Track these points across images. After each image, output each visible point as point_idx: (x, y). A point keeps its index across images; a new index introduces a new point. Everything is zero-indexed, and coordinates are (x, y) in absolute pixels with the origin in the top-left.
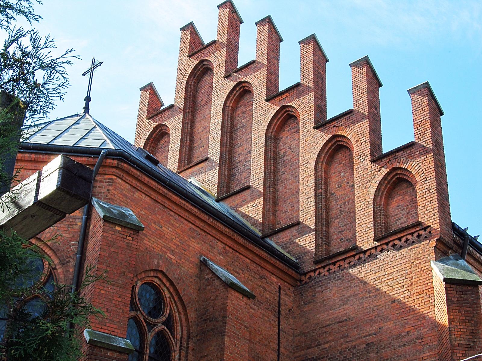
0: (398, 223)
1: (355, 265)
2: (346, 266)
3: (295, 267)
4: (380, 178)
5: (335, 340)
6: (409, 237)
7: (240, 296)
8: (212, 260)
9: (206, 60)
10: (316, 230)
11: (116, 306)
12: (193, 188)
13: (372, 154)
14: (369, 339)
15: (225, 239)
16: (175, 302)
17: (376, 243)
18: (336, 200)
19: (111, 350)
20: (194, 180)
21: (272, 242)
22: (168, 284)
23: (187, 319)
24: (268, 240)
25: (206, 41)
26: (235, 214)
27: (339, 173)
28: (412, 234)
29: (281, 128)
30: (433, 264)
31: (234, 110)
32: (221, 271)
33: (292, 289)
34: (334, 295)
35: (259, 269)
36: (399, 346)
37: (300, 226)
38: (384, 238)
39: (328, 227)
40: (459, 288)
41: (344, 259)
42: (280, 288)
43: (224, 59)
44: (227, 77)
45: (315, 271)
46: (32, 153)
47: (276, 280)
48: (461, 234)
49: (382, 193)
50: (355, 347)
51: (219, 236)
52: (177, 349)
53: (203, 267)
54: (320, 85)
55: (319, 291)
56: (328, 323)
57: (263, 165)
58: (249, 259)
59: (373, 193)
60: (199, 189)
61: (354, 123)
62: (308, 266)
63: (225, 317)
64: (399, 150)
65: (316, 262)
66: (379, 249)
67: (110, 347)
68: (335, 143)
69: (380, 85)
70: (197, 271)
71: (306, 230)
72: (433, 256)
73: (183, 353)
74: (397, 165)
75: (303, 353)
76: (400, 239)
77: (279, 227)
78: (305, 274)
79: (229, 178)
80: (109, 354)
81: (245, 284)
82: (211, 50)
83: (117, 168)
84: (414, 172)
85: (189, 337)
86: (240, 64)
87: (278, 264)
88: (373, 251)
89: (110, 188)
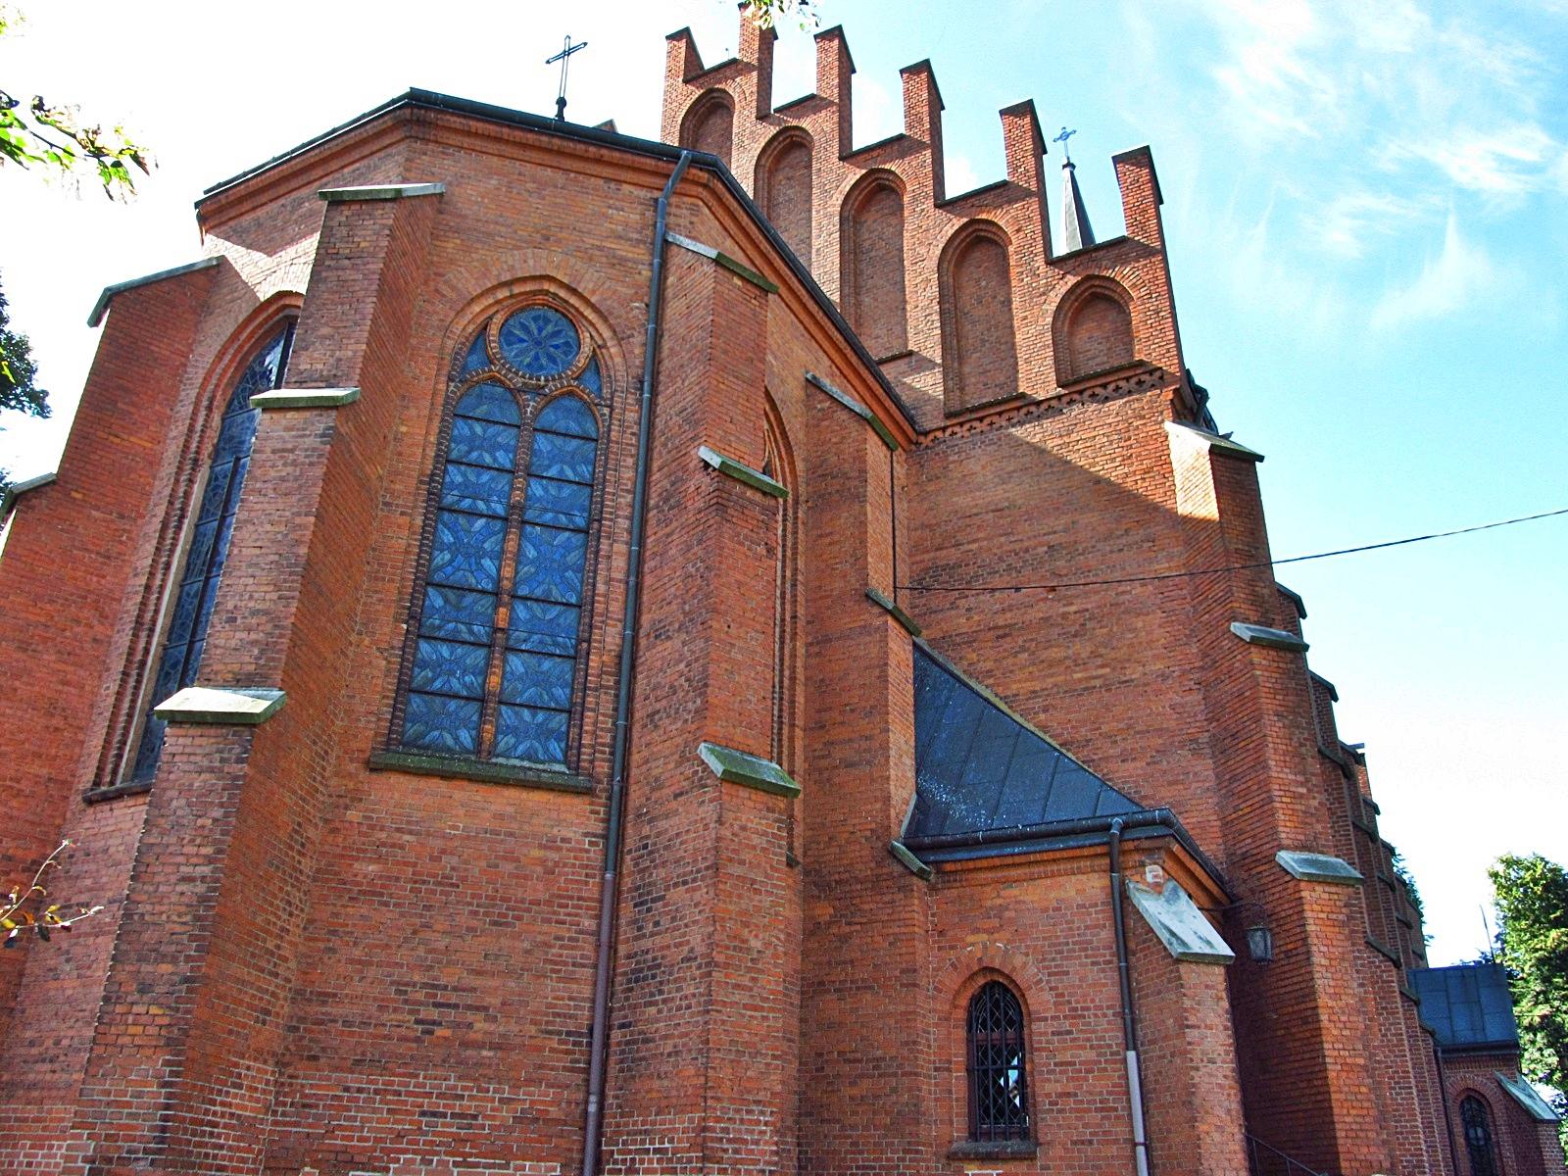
0: (1090, 363)
1: (1021, 423)
2: (1004, 423)
4: (1064, 290)
5: (988, 538)
6: (1122, 384)
9: (718, 90)
10: (944, 365)
11: (744, 413)
14: (1053, 539)
17: (1063, 392)
18: (973, 323)
19: (751, 487)
21: (888, 371)
25: (707, 66)
27: (978, 281)
28: (1127, 379)
34: (983, 468)
36: (1112, 552)
37: (914, 358)
38: (1076, 382)
41: (1000, 414)
43: (755, 89)
45: (944, 429)
46: (553, 136)
50: (1027, 551)
51: (826, 345)
53: (812, 390)
55: (953, 462)
56: (975, 511)
57: (837, 261)
61: (1010, 202)
62: (931, 420)
65: (949, 416)
66: (1065, 400)
67: (752, 482)
70: (802, 394)
71: (925, 364)
72: (1168, 413)
75: (926, 557)
76: (1104, 386)
78: (926, 434)
80: (749, 493)
82: (728, 74)
83: (705, 186)
84: (1126, 285)
89: (694, 219)
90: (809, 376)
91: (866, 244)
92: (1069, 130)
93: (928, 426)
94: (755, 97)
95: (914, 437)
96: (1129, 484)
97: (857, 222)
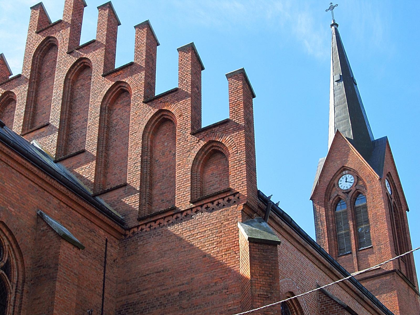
0: (212, 188)
1: (173, 224)
2: (166, 223)
3: (121, 223)
4: (198, 149)
6: (221, 201)
7: (71, 247)
8: (47, 214)
9: (52, 37)
10: (140, 191)
12: (34, 149)
13: (192, 128)
14: (183, 288)
15: (60, 196)
16: (13, 250)
20: (34, 142)
21: (101, 200)
22: (7, 234)
23: (23, 265)
24: (98, 198)
25: (53, 20)
26: (71, 174)
27: (163, 143)
28: (223, 198)
29: (115, 100)
30: (239, 225)
31: (74, 82)
32: (55, 224)
33: (117, 242)
34: (153, 249)
35: (89, 223)
36: (208, 295)
37: (127, 187)
38: (199, 201)
39: (151, 189)
40: (261, 247)
42: (107, 241)
43: (68, 37)
44: (70, 53)
45: (138, 227)
47: (104, 234)
48: (265, 200)
49: (199, 162)
51: (55, 193)
52: (13, 291)
53: (40, 220)
54: (151, 65)
56: (148, 272)
58: (81, 214)
59: (191, 162)
60: (40, 151)
61: (178, 100)
62: (132, 223)
63: (57, 264)
64: (215, 125)
66: (194, 210)
68: (160, 117)
69: (203, 68)
72: (240, 218)
73: (19, 295)
74: (214, 139)
75: (124, 298)
77: (108, 187)
78: (129, 229)
79: (67, 142)
81: (76, 236)
82: (57, 28)
84: (227, 145)
85: (24, 281)
86: (82, 43)
87: (106, 219)
88: (189, 212)
90: (38, 213)
91: (114, 122)
92: (334, 5)
93: (130, 225)
94: (68, 41)
95: (123, 231)
96: (219, 258)
97: (110, 110)
